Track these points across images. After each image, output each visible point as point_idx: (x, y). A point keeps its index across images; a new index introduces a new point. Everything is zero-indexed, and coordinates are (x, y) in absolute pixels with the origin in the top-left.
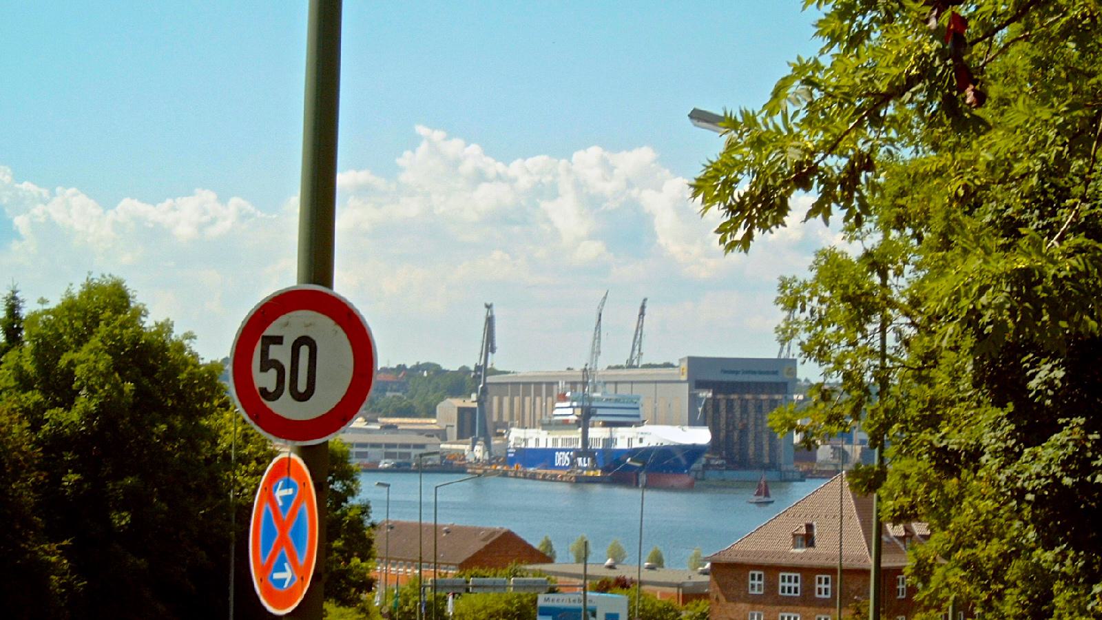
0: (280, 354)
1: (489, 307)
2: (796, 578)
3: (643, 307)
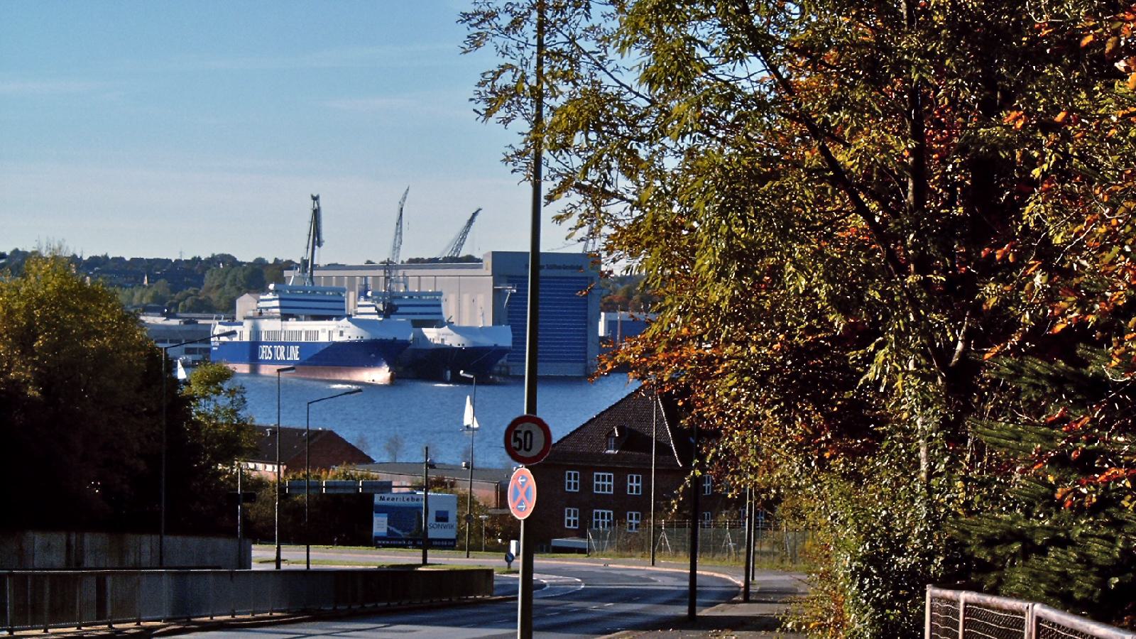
0: (521, 436)
1: (315, 199)
2: (610, 477)
3: (475, 214)
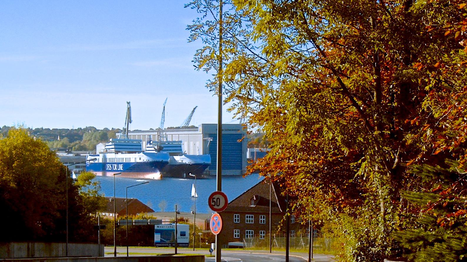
0: (215, 200)
1: (128, 103)
